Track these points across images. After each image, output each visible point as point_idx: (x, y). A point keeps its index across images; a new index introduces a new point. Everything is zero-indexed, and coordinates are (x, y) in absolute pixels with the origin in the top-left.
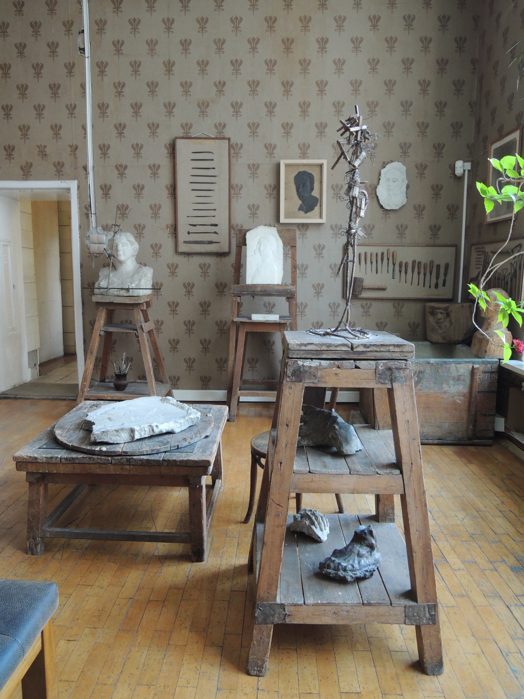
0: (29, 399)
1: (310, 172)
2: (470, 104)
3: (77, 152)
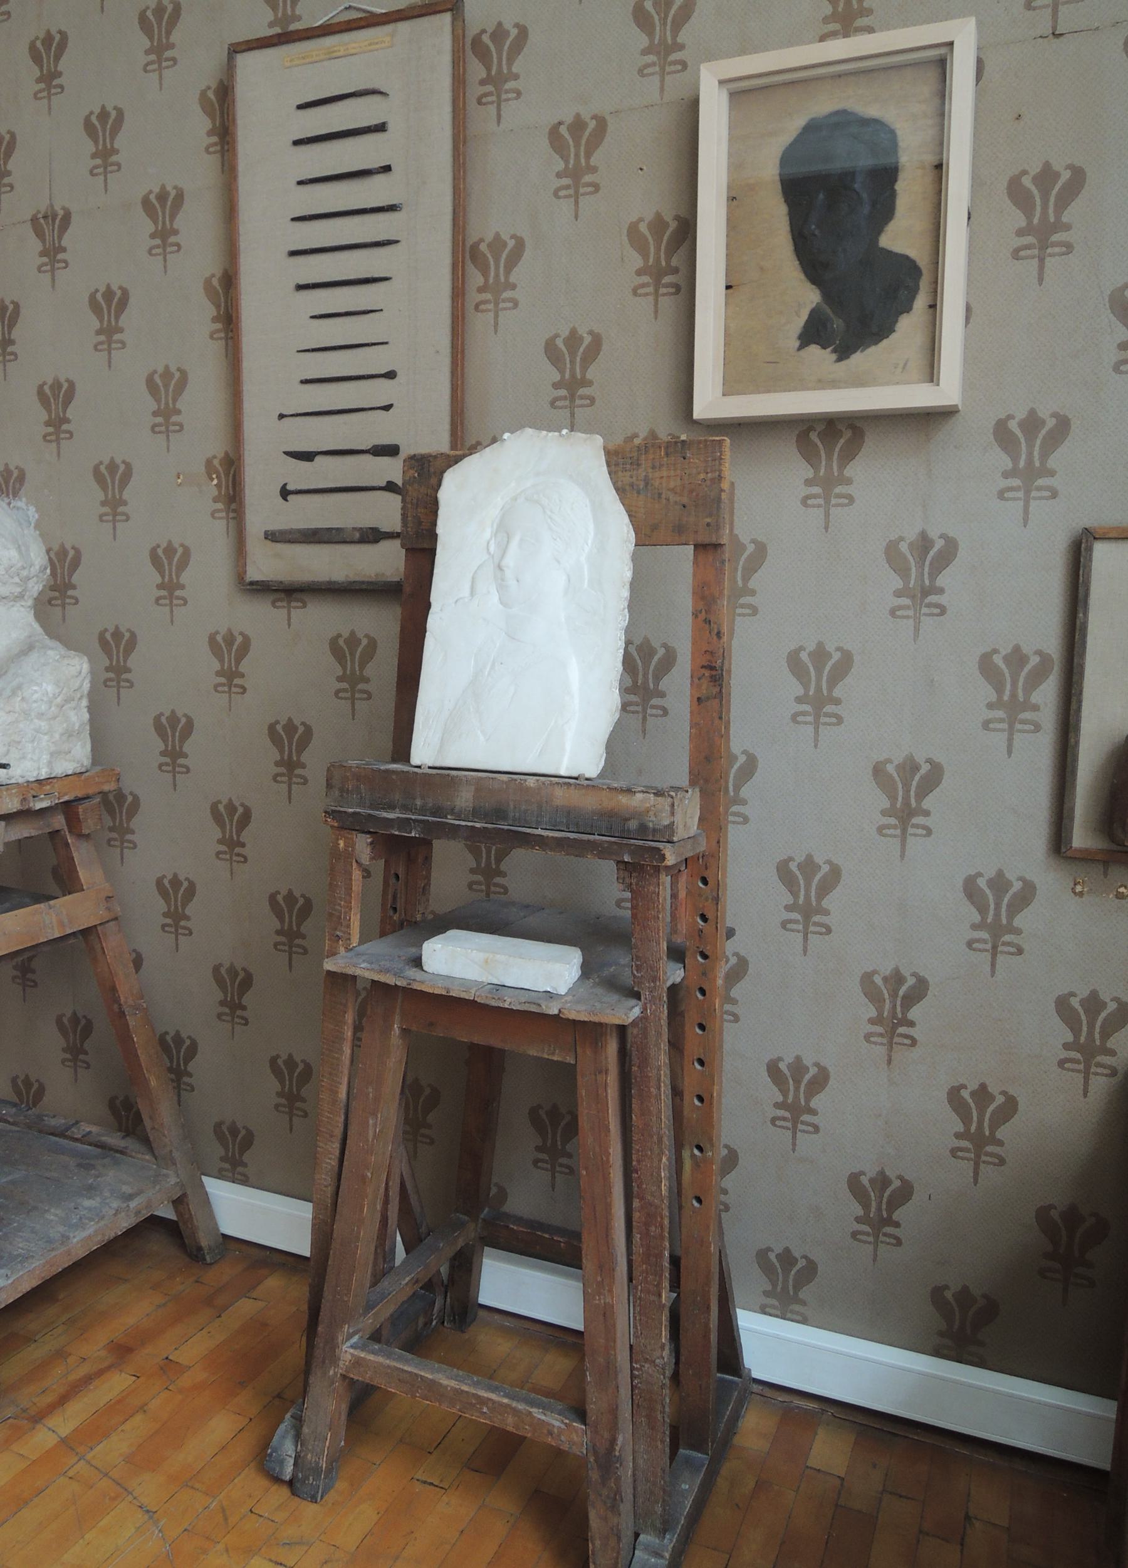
1: (872, 111)
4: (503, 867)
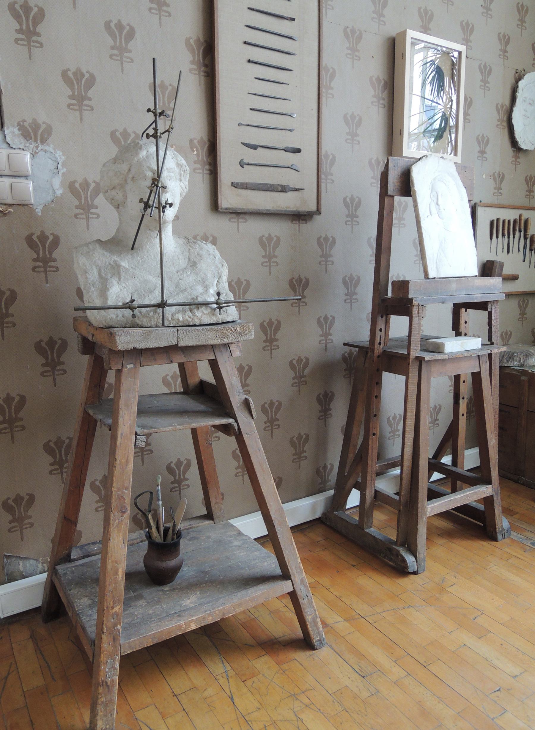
4: (331, 331)
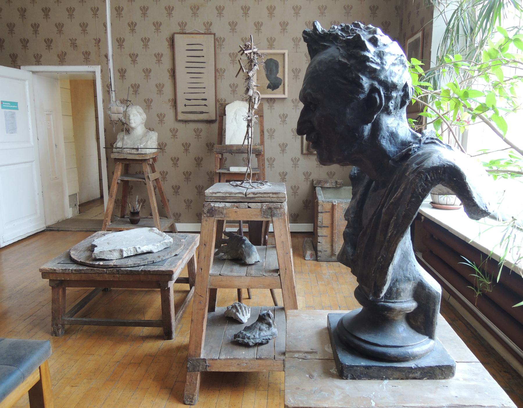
0: (68, 231)
1: (275, 59)
2: (396, 8)
3: (100, 44)
